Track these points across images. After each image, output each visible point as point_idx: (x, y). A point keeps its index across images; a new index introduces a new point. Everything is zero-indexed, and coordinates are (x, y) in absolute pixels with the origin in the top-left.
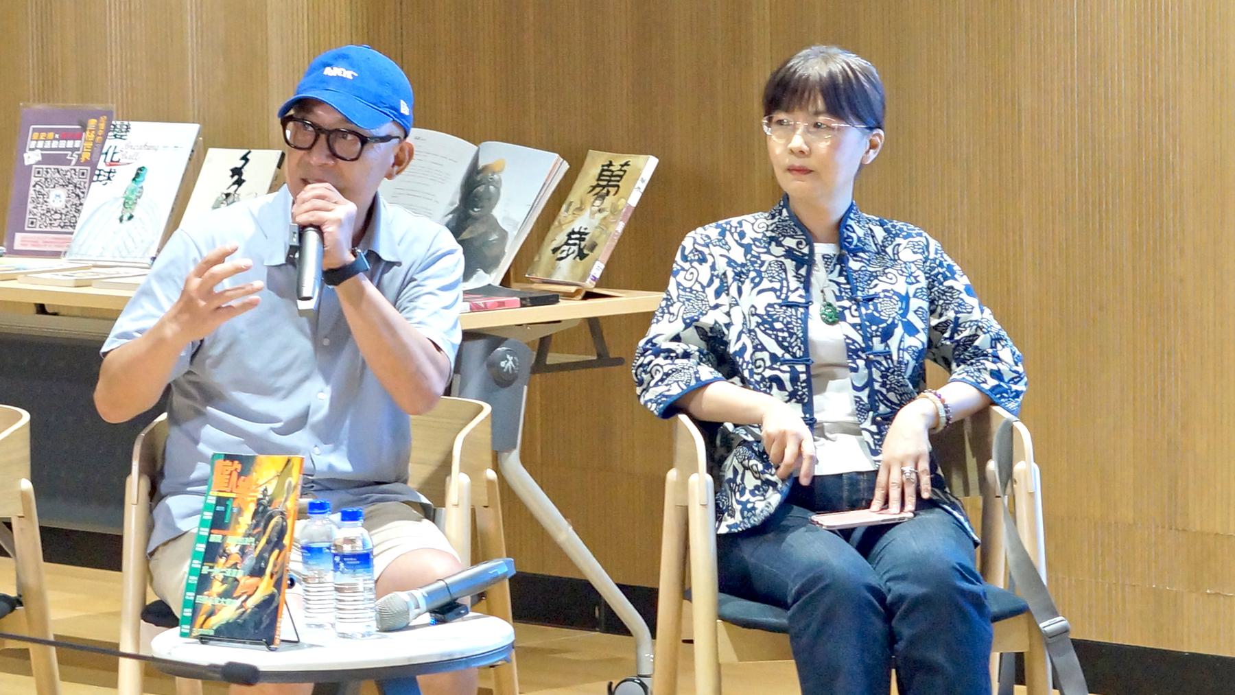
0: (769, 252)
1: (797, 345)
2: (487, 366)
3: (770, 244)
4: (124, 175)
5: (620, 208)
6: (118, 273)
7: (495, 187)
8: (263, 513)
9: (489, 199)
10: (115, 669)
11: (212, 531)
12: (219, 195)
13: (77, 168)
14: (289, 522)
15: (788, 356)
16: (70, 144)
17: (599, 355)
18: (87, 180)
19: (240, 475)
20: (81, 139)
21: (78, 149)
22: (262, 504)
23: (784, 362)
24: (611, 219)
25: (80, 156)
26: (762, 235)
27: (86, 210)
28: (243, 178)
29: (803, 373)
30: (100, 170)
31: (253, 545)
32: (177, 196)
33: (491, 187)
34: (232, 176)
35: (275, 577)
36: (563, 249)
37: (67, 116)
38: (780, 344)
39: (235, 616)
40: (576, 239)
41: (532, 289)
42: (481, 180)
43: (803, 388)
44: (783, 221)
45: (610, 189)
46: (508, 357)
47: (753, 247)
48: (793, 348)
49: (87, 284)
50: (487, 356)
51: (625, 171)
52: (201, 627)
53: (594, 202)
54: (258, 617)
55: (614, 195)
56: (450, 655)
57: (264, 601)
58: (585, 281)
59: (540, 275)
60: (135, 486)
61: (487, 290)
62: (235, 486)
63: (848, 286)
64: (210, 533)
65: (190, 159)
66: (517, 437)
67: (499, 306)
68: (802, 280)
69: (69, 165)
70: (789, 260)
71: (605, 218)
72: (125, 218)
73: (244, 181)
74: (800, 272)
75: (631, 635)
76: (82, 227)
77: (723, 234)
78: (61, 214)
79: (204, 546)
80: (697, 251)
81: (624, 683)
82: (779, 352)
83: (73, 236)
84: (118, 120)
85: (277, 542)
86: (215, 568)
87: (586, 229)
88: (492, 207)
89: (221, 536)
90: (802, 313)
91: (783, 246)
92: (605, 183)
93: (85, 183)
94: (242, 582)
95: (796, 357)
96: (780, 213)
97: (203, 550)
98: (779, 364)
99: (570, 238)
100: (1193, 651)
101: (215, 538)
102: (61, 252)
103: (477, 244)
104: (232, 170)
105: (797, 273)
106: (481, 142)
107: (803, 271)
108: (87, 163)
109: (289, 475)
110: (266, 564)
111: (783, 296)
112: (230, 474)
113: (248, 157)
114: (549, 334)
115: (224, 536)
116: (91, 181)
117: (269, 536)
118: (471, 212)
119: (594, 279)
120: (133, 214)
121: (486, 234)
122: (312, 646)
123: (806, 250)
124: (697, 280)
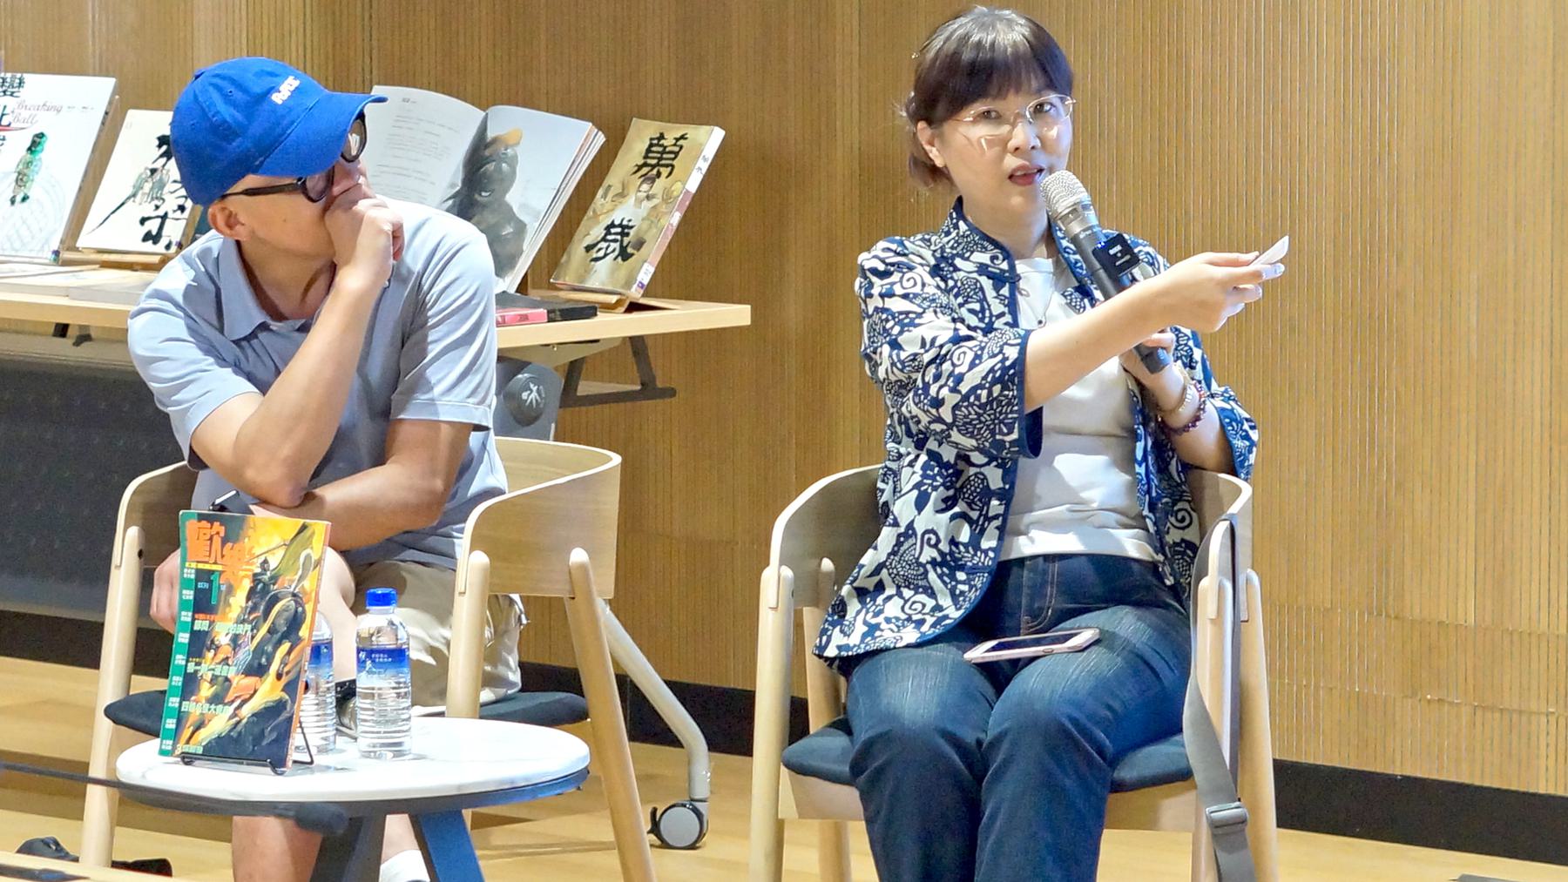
5: (675, 194)
7: (509, 165)
8: (263, 593)
9: (502, 180)
10: (82, 795)
11: (196, 616)
17: (642, 384)
19: (224, 541)
22: (260, 581)
24: (664, 208)
31: (249, 634)
33: (504, 165)
34: (160, 146)
35: (285, 680)
36: (599, 246)
39: (228, 728)
41: (557, 296)
42: (491, 156)
45: (662, 169)
46: (532, 386)
51: (681, 147)
52: (188, 742)
53: (640, 186)
54: (256, 730)
55: (667, 177)
56: (512, 782)
57: (265, 708)
58: (630, 289)
59: (569, 278)
64: (194, 620)
65: (103, 123)
67: (520, 321)
68: (1006, 302)
71: (654, 207)
72: (19, 199)
74: (1001, 292)
81: (672, 810)
86: (203, 665)
87: (630, 221)
88: (506, 191)
89: (208, 622)
92: (654, 162)
94: (234, 684)
97: (187, 641)
99: (608, 233)
101: (201, 625)
104: (159, 139)
106: (488, 107)
107: (1005, 291)
109: (308, 543)
110: (269, 663)
111: (987, 320)
114: (581, 356)
117: (273, 623)
118: (477, 196)
123: (1005, 266)
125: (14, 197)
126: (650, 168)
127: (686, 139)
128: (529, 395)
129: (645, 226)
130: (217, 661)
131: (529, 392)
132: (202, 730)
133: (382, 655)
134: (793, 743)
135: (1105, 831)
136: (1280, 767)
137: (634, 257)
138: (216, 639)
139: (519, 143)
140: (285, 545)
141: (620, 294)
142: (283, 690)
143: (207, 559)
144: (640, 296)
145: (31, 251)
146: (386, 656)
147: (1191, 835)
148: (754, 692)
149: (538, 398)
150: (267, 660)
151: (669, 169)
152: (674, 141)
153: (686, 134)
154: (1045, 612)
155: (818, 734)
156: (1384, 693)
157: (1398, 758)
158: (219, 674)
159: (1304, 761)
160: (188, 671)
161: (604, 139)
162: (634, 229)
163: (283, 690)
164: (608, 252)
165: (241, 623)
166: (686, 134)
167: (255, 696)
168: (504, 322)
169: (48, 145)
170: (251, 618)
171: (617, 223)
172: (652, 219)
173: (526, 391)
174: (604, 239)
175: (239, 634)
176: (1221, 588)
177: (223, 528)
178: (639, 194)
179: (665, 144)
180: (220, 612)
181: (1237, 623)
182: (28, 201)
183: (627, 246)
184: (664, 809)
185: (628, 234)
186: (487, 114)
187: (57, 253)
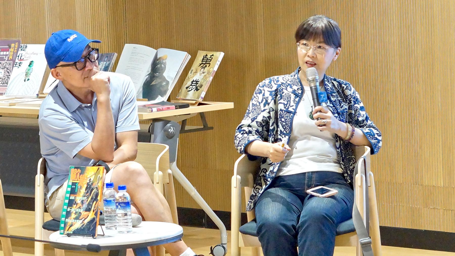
0: (286, 89)
1: (287, 128)
2: (164, 131)
3: (288, 86)
4: (25, 64)
5: (211, 71)
8: (89, 188)
9: (162, 70)
11: (71, 195)
13: (8, 62)
16: (5, 53)
18: (12, 66)
19: (80, 174)
20: (9, 51)
21: (8, 55)
22: (89, 185)
24: (208, 76)
25: (8, 57)
27: (12, 77)
30: (16, 63)
31: (86, 200)
32: (45, 71)
33: (162, 65)
35: (95, 212)
36: (190, 87)
38: (283, 127)
40: (195, 83)
41: (179, 102)
42: (158, 63)
44: (295, 79)
45: (207, 65)
46: (171, 127)
47: (281, 86)
48: (286, 129)
49: (14, 104)
50: (164, 128)
51: (212, 58)
52: (68, 230)
53: (201, 70)
54: (88, 227)
55: (208, 67)
56: (160, 239)
59: (182, 97)
60: (39, 178)
61: (162, 103)
62: (79, 178)
64: (70, 196)
67: (167, 109)
68: (296, 103)
69: (5, 61)
71: (205, 76)
72: (26, 80)
74: (296, 100)
75: (219, 229)
76: (10, 84)
78: (2, 79)
79: (68, 201)
80: (259, 89)
82: (283, 130)
83: (7, 87)
84: (22, 44)
85: (95, 199)
86: (73, 209)
87: (198, 80)
89: (74, 197)
90: (291, 116)
91: (292, 88)
92: (205, 63)
94: (82, 214)
96: (295, 76)
97: (68, 202)
98: (282, 134)
99: (192, 83)
100: (426, 229)
101: (72, 198)
102: (3, 93)
103: (158, 86)
105: (294, 100)
107: (297, 99)
108: (11, 60)
109: (99, 173)
110: (91, 207)
111: (287, 108)
112: (77, 174)
115: (75, 197)
116: (13, 67)
117: (92, 196)
118: (155, 74)
119: (202, 98)
120: (29, 78)
121: (161, 82)
122: (109, 236)
124: (258, 101)
125: (25, 79)
126: (203, 64)
127: (213, 56)
128: (171, 130)
129: (203, 81)
130: (77, 208)
131: (170, 129)
132: (72, 227)
133: (123, 204)
134: (242, 225)
135: (336, 248)
136: (381, 228)
138: (76, 201)
139: (166, 59)
140: (95, 174)
141: (196, 100)
142: (94, 215)
143: (75, 179)
145: (30, 94)
146: (124, 204)
147: (356, 247)
148: (231, 212)
149: (173, 131)
151: (209, 64)
152: (210, 56)
154: (312, 186)
155: (250, 222)
156: (418, 207)
157: (423, 225)
158: (77, 211)
159: (386, 226)
160: (68, 211)
161: (191, 57)
163: (94, 215)
164: (192, 89)
165: (84, 197)
167: (88, 217)
168: (163, 110)
169: (34, 65)
170: (87, 195)
171: (195, 80)
173: (170, 129)
174: (191, 85)
175: (83, 200)
176: (362, 177)
177: (80, 170)
178: (201, 72)
179: (208, 58)
180: (78, 194)
181: (367, 187)
182: (29, 80)
183: (198, 87)
184: (214, 247)
185: (198, 84)
186: (157, 51)
187: (38, 95)
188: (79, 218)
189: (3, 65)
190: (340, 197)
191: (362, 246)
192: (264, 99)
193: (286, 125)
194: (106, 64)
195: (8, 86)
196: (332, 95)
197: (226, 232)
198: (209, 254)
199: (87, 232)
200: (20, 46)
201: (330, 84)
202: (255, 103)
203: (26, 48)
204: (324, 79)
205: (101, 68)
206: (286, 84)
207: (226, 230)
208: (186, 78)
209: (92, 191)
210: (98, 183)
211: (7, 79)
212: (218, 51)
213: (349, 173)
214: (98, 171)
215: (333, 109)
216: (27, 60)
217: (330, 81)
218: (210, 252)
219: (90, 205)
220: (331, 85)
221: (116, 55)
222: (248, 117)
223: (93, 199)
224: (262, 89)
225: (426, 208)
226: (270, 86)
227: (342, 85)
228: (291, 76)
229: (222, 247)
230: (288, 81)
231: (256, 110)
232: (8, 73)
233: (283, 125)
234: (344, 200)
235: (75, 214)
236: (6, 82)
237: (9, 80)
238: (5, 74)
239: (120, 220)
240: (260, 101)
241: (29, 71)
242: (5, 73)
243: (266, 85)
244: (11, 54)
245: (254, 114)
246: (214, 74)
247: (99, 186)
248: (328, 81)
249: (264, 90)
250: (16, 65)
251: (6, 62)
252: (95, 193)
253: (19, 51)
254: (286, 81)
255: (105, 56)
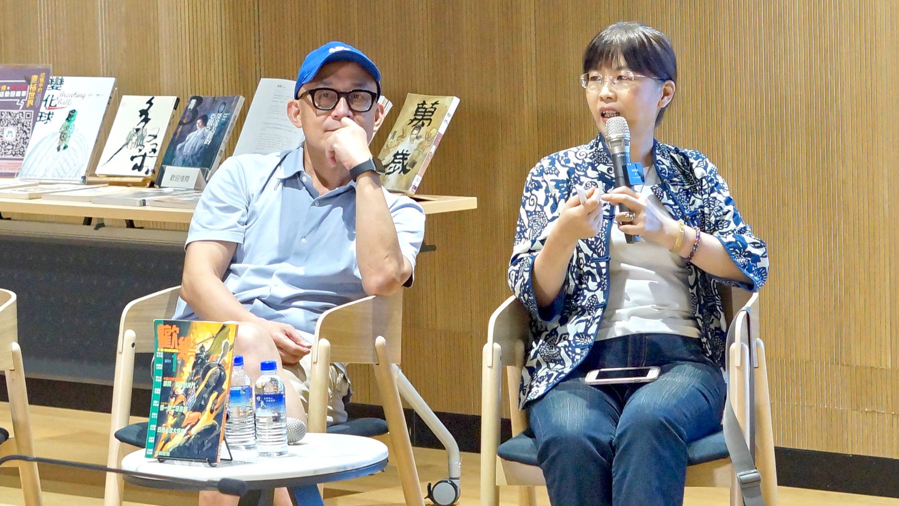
0: (586, 175)
3: (587, 168)
5: (433, 135)
6: (59, 189)
8: (201, 364)
10: (103, 483)
11: (164, 379)
12: (131, 130)
13: (24, 111)
14: (228, 372)
15: (595, 256)
16: (18, 94)
18: (32, 120)
19: (179, 336)
20: (27, 90)
21: (24, 98)
22: (200, 358)
23: (593, 260)
25: (26, 102)
26: (582, 161)
27: (32, 142)
28: (149, 117)
29: (604, 268)
30: (42, 113)
31: (194, 388)
34: (141, 116)
35: (215, 413)
36: (390, 166)
37: (16, 73)
38: (589, 246)
39: (184, 441)
43: (605, 279)
44: (599, 151)
45: (425, 122)
47: (576, 171)
49: (38, 196)
51: (435, 109)
52: (161, 450)
53: (413, 131)
55: (428, 126)
56: (345, 468)
57: (205, 430)
63: (677, 207)
64: (163, 380)
65: (109, 103)
66: (360, 302)
69: (19, 109)
70: (601, 182)
71: (421, 143)
72: (62, 147)
73: (149, 119)
77: (552, 163)
78: (13, 145)
79: (160, 390)
80: (533, 180)
82: (590, 253)
83: (23, 162)
84: (54, 75)
86: (169, 406)
87: (407, 151)
89: (171, 382)
90: (606, 224)
91: (597, 171)
92: (420, 117)
93: (30, 122)
95: (600, 257)
96: (597, 145)
97: (159, 393)
100: (856, 453)
101: (167, 384)
104: (140, 111)
108: (31, 107)
110: (206, 404)
113: (153, 101)
116: (35, 121)
117: (208, 381)
120: (68, 145)
125: (59, 146)
126: (418, 121)
127: (438, 104)
129: (416, 154)
135: (686, 489)
137: (410, 172)
138: (176, 391)
140: (213, 337)
142: (214, 419)
144: (414, 193)
145: (70, 177)
150: (205, 402)
153: (438, 101)
158: (178, 411)
160: (161, 410)
161: (392, 105)
162: (410, 156)
163: (214, 419)
164: (395, 169)
165: (190, 382)
166: (438, 101)
169: (78, 117)
170: (195, 379)
171: (400, 152)
172: (420, 149)
174: (393, 162)
175: (189, 389)
177: (178, 328)
178: (412, 136)
179: (426, 107)
185: (406, 159)
187: (84, 178)
188: (181, 425)
189: (15, 117)
190: (696, 387)
191: (741, 486)
192: (549, 198)
193: (595, 241)
194: (222, 117)
195: (24, 160)
196: (671, 181)
197: (458, 454)
198: (425, 498)
199: (197, 453)
200: (50, 81)
201: (666, 159)
202: (532, 209)
203: (61, 84)
204: (654, 149)
205: (212, 126)
206: (584, 164)
207: (458, 450)
208: (382, 147)
209: (207, 372)
210: (222, 357)
211: (23, 145)
212: (447, 95)
213: (710, 337)
214: (223, 331)
215: (673, 209)
216: (63, 108)
217: (666, 154)
218: (427, 494)
219: (203, 398)
220: (668, 161)
221: (242, 99)
222: (523, 240)
223: (211, 388)
224: (539, 179)
225: (857, 410)
226: (554, 171)
227: (690, 159)
228: (589, 147)
229: (450, 484)
230: (586, 158)
231: (537, 221)
232: (25, 133)
233: (590, 243)
234: (703, 392)
235: (173, 416)
236: (19, 151)
237: (27, 147)
238: (19, 136)
239: (265, 429)
240: (541, 201)
241: (66, 129)
242: (18, 133)
243: (545, 170)
244: (31, 97)
245: (536, 230)
246: (440, 140)
247: (227, 362)
248: (663, 155)
249: (545, 181)
250: (42, 118)
251: (20, 112)
252: (215, 375)
253: (47, 91)
254: (583, 159)
255: (221, 102)
